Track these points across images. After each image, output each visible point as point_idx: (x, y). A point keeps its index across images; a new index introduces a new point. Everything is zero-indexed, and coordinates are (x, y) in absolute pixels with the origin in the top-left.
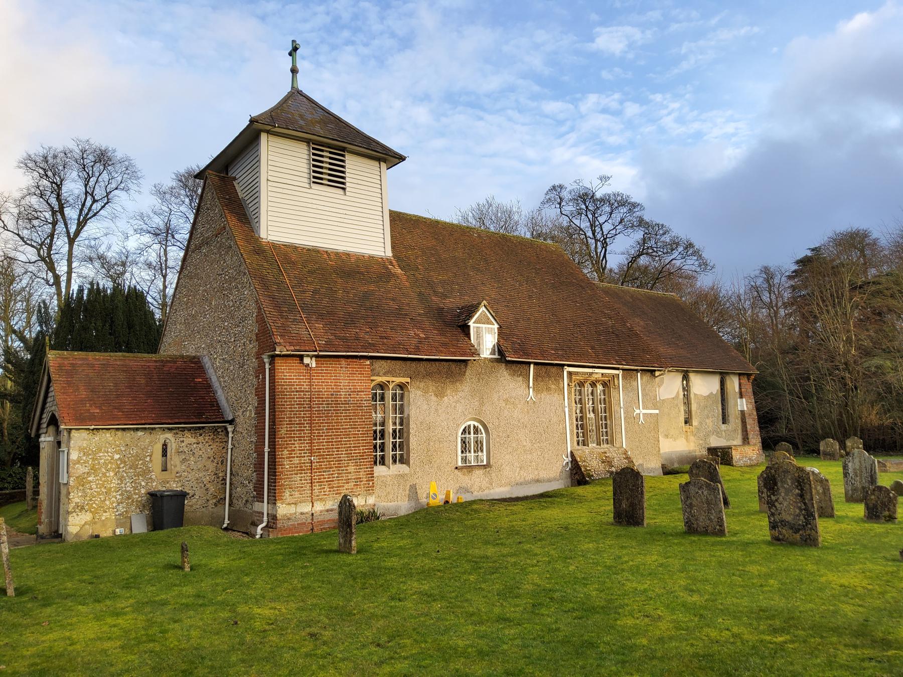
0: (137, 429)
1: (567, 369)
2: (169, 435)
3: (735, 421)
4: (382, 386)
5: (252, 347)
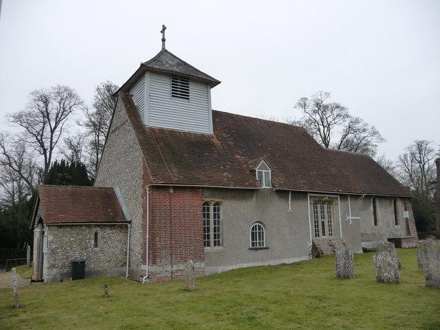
0: (145, 229)
3: (402, 224)
4: (207, 203)
5: (141, 182)
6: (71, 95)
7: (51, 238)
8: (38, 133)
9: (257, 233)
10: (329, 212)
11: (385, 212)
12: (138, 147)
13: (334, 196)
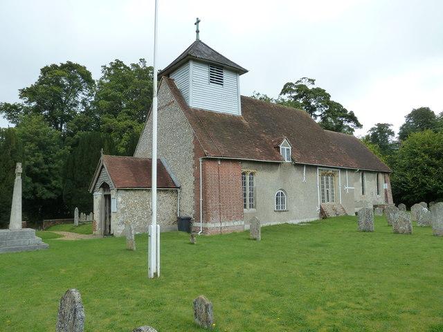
3: (382, 194)
4: (244, 174)
5: (192, 155)
9: (280, 199)
10: (332, 183)
11: (370, 182)
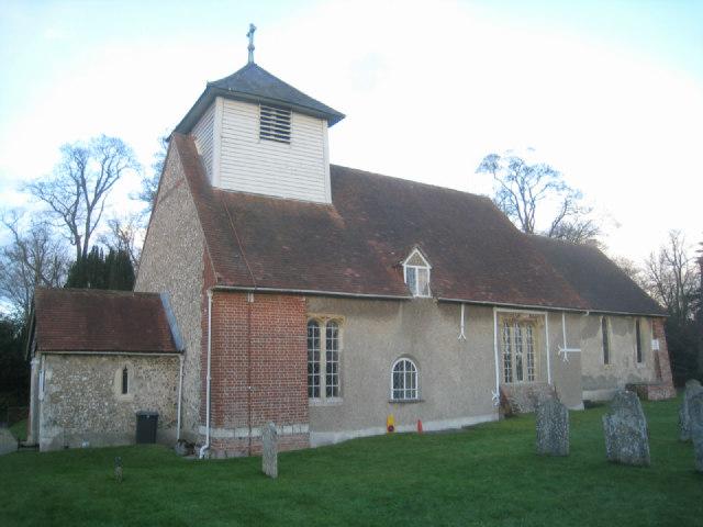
0: (102, 355)
1: (496, 310)
2: (128, 362)
4: (314, 323)
6: (121, 150)
7: (49, 375)
8: (69, 211)
11: (621, 342)
12: (197, 222)
13: (539, 313)
